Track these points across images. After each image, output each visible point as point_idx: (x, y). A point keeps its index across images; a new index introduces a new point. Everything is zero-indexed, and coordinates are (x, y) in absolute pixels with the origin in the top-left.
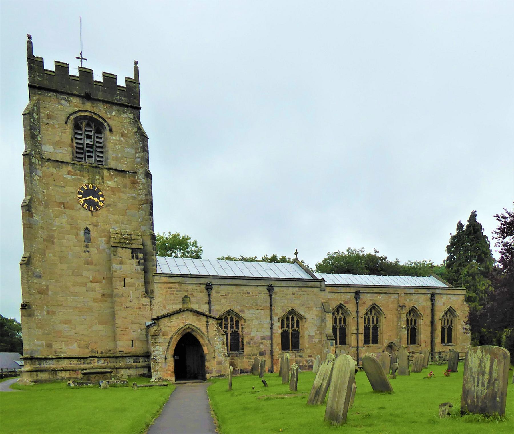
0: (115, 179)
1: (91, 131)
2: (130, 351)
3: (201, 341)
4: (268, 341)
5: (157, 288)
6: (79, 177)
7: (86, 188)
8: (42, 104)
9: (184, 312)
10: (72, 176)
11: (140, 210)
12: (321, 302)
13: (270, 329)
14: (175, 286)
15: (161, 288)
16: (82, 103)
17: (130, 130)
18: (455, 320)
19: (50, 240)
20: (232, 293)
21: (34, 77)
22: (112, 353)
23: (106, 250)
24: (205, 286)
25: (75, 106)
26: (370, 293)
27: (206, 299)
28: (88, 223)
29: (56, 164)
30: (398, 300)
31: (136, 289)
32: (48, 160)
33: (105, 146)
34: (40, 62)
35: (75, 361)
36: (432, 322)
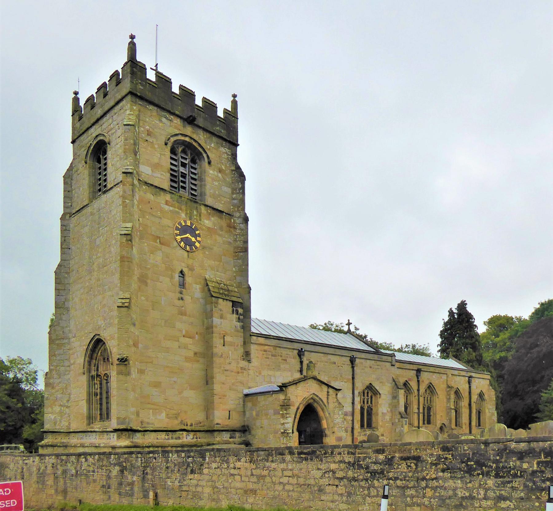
0: (212, 219)
1: (186, 159)
2: (227, 423)
3: (321, 413)
4: (350, 417)
5: (253, 349)
6: (177, 210)
7: (184, 224)
8: (142, 117)
9: (309, 380)
10: (170, 207)
11: (236, 258)
12: (392, 378)
13: (351, 404)
14: (271, 349)
15: (257, 350)
16: (182, 125)
17: (226, 166)
18: (483, 404)
19: (143, 280)
20: (320, 362)
21: (137, 84)
22: (201, 426)
23: (201, 300)
24: (297, 351)
25: (176, 128)
26: (427, 371)
27: (298, 367)
28: (183, 264)
29: (155, 190)
30: (447, 381)
31: (235, 350)
32: (146, 183)
33: (201, 180)
34: (143, 69)
35: (163, 435)
36: (470, 405)
